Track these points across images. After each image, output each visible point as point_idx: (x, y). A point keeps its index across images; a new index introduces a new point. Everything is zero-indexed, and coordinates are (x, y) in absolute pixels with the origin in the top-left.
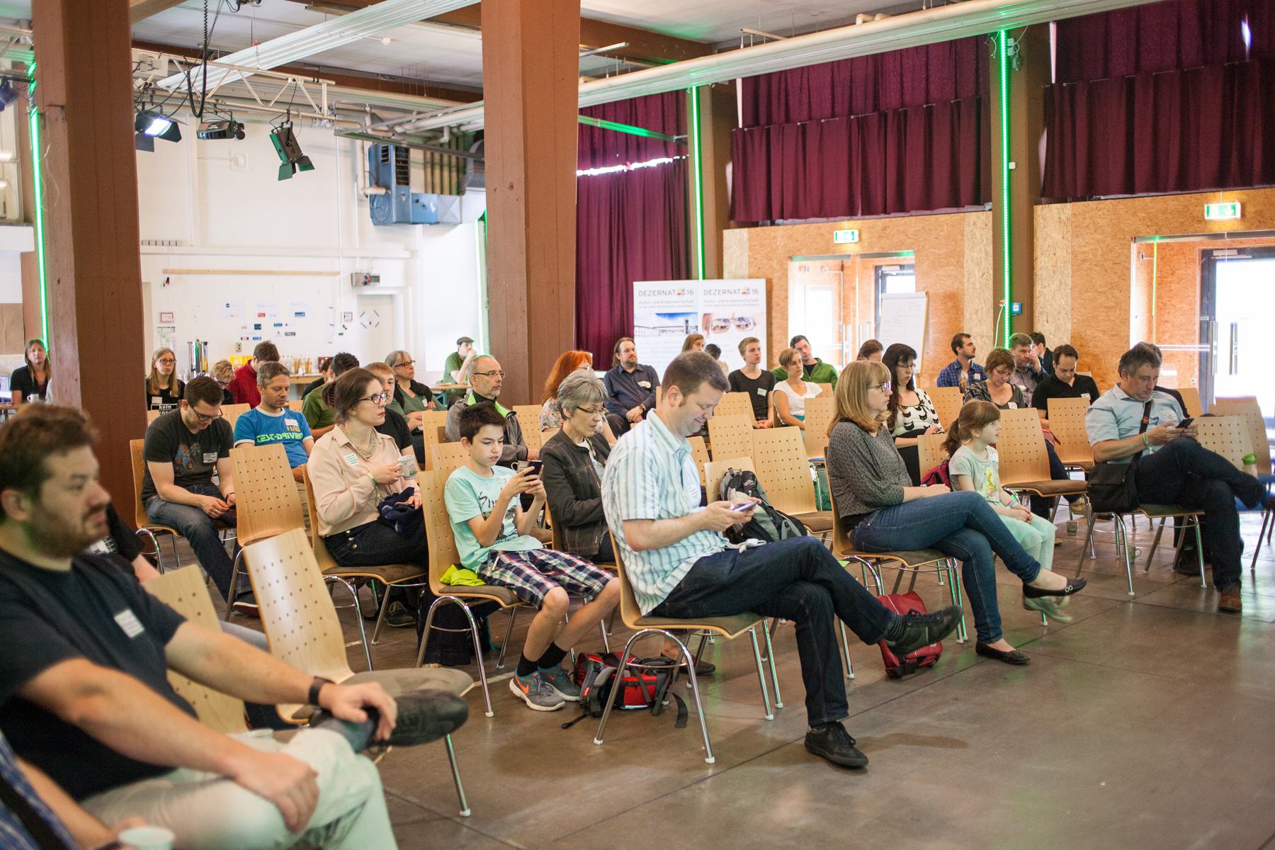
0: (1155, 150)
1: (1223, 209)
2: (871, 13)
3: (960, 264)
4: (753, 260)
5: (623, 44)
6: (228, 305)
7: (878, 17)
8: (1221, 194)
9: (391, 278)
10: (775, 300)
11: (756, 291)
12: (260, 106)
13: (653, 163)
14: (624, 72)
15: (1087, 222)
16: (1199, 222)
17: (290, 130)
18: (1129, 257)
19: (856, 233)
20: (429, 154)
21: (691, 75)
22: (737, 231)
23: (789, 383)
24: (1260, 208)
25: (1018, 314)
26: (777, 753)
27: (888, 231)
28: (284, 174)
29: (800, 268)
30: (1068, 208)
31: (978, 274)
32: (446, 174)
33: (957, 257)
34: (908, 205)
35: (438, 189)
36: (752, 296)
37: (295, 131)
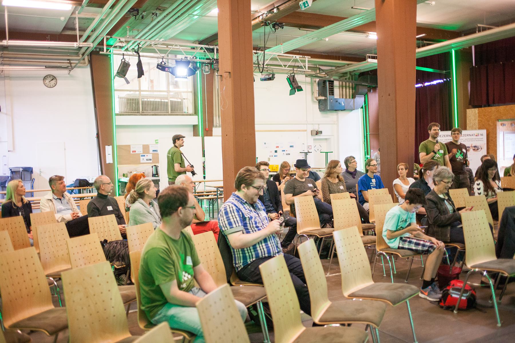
4: (480, 122)
5: (424, 35)
9: (326, 132)
11: (482, 135)
12: (284, 68)
13: (435, 82)
14: (424, 46)
17: (294, 76)
20: (341, 82)
21: (452, 45)
22: (473, 109)
28: (292, 93)
32: (348, 90)
35: (344, 97)
36: (480, 137)
37: (296, 76)
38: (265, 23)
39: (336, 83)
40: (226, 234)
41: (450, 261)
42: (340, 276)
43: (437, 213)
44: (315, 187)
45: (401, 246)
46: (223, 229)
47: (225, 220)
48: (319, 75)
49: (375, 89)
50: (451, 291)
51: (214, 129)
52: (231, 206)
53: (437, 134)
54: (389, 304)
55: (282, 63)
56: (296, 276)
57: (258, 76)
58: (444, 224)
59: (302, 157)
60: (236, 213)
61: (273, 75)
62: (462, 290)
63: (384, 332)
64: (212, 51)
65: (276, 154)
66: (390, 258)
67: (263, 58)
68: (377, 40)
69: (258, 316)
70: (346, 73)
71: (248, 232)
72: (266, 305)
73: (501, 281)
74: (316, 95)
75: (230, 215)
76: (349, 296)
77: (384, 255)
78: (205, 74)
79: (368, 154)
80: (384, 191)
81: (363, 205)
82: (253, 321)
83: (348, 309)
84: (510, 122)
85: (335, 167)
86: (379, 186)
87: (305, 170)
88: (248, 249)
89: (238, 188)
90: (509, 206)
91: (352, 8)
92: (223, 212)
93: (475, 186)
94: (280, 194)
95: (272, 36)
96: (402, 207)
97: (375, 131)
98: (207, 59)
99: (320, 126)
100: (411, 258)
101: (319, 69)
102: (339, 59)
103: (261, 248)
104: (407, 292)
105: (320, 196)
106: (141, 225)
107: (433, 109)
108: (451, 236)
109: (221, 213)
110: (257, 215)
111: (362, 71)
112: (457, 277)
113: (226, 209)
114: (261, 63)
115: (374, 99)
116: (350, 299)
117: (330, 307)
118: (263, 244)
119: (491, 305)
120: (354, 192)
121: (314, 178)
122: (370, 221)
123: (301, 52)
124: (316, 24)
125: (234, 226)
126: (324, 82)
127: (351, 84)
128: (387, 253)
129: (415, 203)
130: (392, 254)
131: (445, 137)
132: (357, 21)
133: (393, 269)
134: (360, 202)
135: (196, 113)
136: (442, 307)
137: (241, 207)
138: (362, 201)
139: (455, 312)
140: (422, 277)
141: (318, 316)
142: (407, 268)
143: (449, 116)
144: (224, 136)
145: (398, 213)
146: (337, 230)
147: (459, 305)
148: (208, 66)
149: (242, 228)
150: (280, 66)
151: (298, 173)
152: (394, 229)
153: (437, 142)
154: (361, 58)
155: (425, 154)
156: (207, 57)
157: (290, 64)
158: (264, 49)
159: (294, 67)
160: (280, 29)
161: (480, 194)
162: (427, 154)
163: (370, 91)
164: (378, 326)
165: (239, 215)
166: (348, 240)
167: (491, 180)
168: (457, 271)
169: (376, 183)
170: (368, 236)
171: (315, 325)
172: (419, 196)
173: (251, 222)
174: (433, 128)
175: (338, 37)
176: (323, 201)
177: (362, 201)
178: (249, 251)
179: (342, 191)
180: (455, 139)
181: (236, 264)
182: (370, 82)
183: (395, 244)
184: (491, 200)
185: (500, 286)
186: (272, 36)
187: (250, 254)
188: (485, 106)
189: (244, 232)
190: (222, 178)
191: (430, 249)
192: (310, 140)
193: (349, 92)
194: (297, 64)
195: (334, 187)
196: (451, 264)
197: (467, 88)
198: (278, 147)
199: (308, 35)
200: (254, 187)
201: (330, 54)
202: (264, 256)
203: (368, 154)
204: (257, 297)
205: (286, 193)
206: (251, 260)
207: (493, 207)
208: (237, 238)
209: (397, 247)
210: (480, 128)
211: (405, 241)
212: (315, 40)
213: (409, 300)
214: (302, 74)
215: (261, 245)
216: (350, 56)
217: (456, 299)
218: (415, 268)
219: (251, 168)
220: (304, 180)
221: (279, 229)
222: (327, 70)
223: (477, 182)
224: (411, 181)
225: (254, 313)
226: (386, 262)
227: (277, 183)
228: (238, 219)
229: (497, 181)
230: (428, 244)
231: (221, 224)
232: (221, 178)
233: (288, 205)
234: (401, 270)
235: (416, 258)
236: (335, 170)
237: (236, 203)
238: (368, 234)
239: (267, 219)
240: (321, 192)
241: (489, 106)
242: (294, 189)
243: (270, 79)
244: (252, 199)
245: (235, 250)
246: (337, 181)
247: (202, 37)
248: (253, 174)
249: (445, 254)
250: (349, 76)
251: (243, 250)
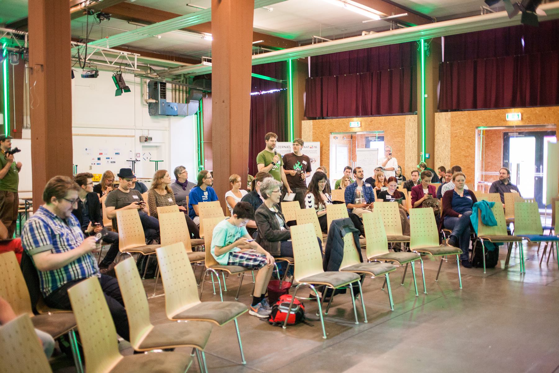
0: (486, 90)
1: (514, 116)
2: (369, 30)
3: (404, 137)
4: (314, 134)
6: (86, 149)
7: (371, 32)
8: (513, 110)
9: (157, 138)
10: (324, 151)
11: (316, 147)
12: (109, 65)
13: (271, 91)
14: (261, 52)
15: (457, 120)
16: (504, 121)
17: (121, 75)
18: (474, 135)
19: (359, 123)
20: (174, 85)
21: (288, 54)
22: (308, 121)
23: (233, 192)
24: (529, 115)
25: (428, 158)
28: (118, 93)
29: (334, 137)
30: (449, 114)
31: (411, 142)
32: (181, 94)
33: (402, 134)
35: (177, 101)
36: (314, 149)
37: (123, 75)
38: (88, 11)
39: (169, 86)
40: (31, 254)
41: (281, 276)
42: (164, 297)
43: (269, 227)
44: (141, 199)
45: (231, 261)
46: (28, 248)
47: (30, 237)
48: (149, 75)
49: (209, 94)
50: (281, 306)
51: (24, 131)
52: (37, 222)
53: (274, 145)
54: (216, 325)
55: (107, 59)
56: (115, 300)
57: (78, 72)
58: (275, 239)
59: (128, 166)
60: (44, 230)
61: (97, 72)
62: (291, 306)
63: (212, 353)
64: (22, 37)
65: (99, 162)
66: (220, 275)
67: (84, 52)
68: (213, 43)
69: (70, 348)
70: (180, 75)
71: (58, 251)
72: (77, 334)
73: (328, 294)
74: (146, 97)
75: (36, 232)
76: (173, 318)
77: (213, 272)
78: (14, 64)
79: (201, 164)
80: (216, 204)
81: (193, 219)
82: (64, 354)
83: (171, 333)
84: (342, 135)
85: (162, 177)
86: (212, 198)
87: (129, 181)
88: (59, 270)
89: (48, 200)
90: (335, 219)
91: (187, 5)
92: (28, 228)
93: (307, 199)
94: (101, 207)
95: (96, 27)
96: (229, 221)
97: (209, 140)
98: (16, 47)
99: (150, 132)
100: (242, 274)
101: (151, 68)
102: (172, 60)
103: (74, 269)
104: (235, 310)
105: (147, 209)
107: (267, 119)
108: (281, 250)
109: (25, 229)
110: (70, 232)
111: (198, 74)
112: (286, 292)
113: (31, 225)
114: (82, 57)
115: (208, 104)
116: (174, 321)
117: (152, 332)
118: (77, 265)
119: (318, 318)
120: (184, 205)
121: (140, 189)
122: (201, 236)
123: (130, 48)
124: (148, 19)
125: (41, 244)
126: (156, 84)
127: (185, 88)
128: (216, 270)
129: (243, 218)
130: (222, 271)
131: (283, 148)
132: (192, 20)
133: (223, 287)
134: (190, 216)
136: (271, 324)
137: (50, 222)
138: (191, 214)
139: (284, 327)
140: (253, 294)
141: (137, 341)
142: (238, 285)
143: (252, 130)
144: (34, 139)
145: (225, 227)
146: (164, 245)
147: (288, 321)
148: (16, 55)
149: (51, 246)
150: (105, 62)
151: (122, 183)
152: (222, 245)
153: (276, 153)
154: (197, 61)
155: (263, 165)
156: (14, 45)
157: (116, 60)
158: (86, 41)
159: (121, 64)
160: (105, 20)
161: (310, 207)
162: (265, 166)
163: (205, 96)
164: (203, 348)
165: (47, 232)
166: (173, 256)
167: (321, 193)
168: (287, 286)
169: (208, 196)
170: (198, 252)
171: (136, 352)
172: (247, 210)
173: (61, 240)
174: (271, 139)
175: (170, 35)
176: (149, 215)
177: (191, 214)
178: (60, 273)
179: (171, 204)
180: (296, 151)
181: (43, 288)
183: (224, 260)
184: (321, 213)
185: (327, 298)
186: (96, 27)
187: (61, 276)
188: (319, 119)
189: (54, 251)
190: (31, 189)
191: (261, 264)
192: (139, 147)
193: (183, 96)
194: (125, 62)
195: (162, 200)
196: (281, 279)
197: (436, 93)
198: (101, 154)
199: (138, 30)
200: (68, 200)
201: (162, 53)
202: (77, 278)
203: (201, 164)
204: (67, 326)
205: (107, 206)
206: (62, 283)
207: (323, 220)
208: (44, 258)
209: (226, 263)
210: (314, 141)
211: (236, 256)
212: (146, 36)
213: (237, 318)
214: (131, 73)
215: (73, 266)
216: (186, 57)
217: (286, 313)
218: (246, 285)
219: (63, 177)
220: (128, 191)
221: (95, 247)
222: (159, 71)
223: (308, 195)
224: (244, 193)
225: (66, 344)
226: (216, 279)
227: (99, 195)
228: (46, 236)
229: (327, 194)
230: (260, 259)
231: (25, 243)
232: (31, 188)
233: (109, 219)
234: (231, 287)
235: (247, 274)
236: (162, 180)
237: (44, 217)
238: (198, 250)
239: (81, 236)
240: (147, 205)
241: (323, 118)
242: (117, 201)
243: (92, 76)
244: (64, 213)
245: (43, 273)
246: (165, 192)
247: (11, 20)
248: (66, 185)
249: (275, 269)
250: (182, 78)
251: (52, 273)
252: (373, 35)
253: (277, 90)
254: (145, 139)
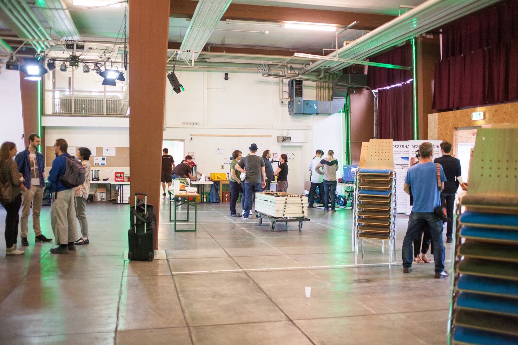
6: (219, 149)
19: (482, 114)
26: (196, 235)
27: (498, 111)
34: (509, 99)
106: (60, 233)
135: (43, 128)
182: (352, 82)
193: (327, 93)
252: (98, 94)
253: (385, 88)
254: (282, 139)
